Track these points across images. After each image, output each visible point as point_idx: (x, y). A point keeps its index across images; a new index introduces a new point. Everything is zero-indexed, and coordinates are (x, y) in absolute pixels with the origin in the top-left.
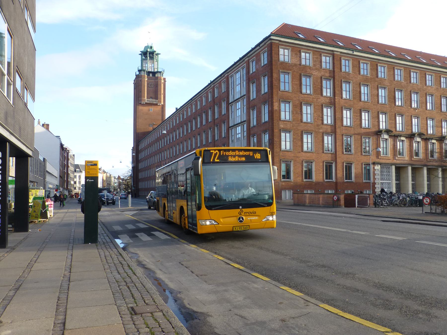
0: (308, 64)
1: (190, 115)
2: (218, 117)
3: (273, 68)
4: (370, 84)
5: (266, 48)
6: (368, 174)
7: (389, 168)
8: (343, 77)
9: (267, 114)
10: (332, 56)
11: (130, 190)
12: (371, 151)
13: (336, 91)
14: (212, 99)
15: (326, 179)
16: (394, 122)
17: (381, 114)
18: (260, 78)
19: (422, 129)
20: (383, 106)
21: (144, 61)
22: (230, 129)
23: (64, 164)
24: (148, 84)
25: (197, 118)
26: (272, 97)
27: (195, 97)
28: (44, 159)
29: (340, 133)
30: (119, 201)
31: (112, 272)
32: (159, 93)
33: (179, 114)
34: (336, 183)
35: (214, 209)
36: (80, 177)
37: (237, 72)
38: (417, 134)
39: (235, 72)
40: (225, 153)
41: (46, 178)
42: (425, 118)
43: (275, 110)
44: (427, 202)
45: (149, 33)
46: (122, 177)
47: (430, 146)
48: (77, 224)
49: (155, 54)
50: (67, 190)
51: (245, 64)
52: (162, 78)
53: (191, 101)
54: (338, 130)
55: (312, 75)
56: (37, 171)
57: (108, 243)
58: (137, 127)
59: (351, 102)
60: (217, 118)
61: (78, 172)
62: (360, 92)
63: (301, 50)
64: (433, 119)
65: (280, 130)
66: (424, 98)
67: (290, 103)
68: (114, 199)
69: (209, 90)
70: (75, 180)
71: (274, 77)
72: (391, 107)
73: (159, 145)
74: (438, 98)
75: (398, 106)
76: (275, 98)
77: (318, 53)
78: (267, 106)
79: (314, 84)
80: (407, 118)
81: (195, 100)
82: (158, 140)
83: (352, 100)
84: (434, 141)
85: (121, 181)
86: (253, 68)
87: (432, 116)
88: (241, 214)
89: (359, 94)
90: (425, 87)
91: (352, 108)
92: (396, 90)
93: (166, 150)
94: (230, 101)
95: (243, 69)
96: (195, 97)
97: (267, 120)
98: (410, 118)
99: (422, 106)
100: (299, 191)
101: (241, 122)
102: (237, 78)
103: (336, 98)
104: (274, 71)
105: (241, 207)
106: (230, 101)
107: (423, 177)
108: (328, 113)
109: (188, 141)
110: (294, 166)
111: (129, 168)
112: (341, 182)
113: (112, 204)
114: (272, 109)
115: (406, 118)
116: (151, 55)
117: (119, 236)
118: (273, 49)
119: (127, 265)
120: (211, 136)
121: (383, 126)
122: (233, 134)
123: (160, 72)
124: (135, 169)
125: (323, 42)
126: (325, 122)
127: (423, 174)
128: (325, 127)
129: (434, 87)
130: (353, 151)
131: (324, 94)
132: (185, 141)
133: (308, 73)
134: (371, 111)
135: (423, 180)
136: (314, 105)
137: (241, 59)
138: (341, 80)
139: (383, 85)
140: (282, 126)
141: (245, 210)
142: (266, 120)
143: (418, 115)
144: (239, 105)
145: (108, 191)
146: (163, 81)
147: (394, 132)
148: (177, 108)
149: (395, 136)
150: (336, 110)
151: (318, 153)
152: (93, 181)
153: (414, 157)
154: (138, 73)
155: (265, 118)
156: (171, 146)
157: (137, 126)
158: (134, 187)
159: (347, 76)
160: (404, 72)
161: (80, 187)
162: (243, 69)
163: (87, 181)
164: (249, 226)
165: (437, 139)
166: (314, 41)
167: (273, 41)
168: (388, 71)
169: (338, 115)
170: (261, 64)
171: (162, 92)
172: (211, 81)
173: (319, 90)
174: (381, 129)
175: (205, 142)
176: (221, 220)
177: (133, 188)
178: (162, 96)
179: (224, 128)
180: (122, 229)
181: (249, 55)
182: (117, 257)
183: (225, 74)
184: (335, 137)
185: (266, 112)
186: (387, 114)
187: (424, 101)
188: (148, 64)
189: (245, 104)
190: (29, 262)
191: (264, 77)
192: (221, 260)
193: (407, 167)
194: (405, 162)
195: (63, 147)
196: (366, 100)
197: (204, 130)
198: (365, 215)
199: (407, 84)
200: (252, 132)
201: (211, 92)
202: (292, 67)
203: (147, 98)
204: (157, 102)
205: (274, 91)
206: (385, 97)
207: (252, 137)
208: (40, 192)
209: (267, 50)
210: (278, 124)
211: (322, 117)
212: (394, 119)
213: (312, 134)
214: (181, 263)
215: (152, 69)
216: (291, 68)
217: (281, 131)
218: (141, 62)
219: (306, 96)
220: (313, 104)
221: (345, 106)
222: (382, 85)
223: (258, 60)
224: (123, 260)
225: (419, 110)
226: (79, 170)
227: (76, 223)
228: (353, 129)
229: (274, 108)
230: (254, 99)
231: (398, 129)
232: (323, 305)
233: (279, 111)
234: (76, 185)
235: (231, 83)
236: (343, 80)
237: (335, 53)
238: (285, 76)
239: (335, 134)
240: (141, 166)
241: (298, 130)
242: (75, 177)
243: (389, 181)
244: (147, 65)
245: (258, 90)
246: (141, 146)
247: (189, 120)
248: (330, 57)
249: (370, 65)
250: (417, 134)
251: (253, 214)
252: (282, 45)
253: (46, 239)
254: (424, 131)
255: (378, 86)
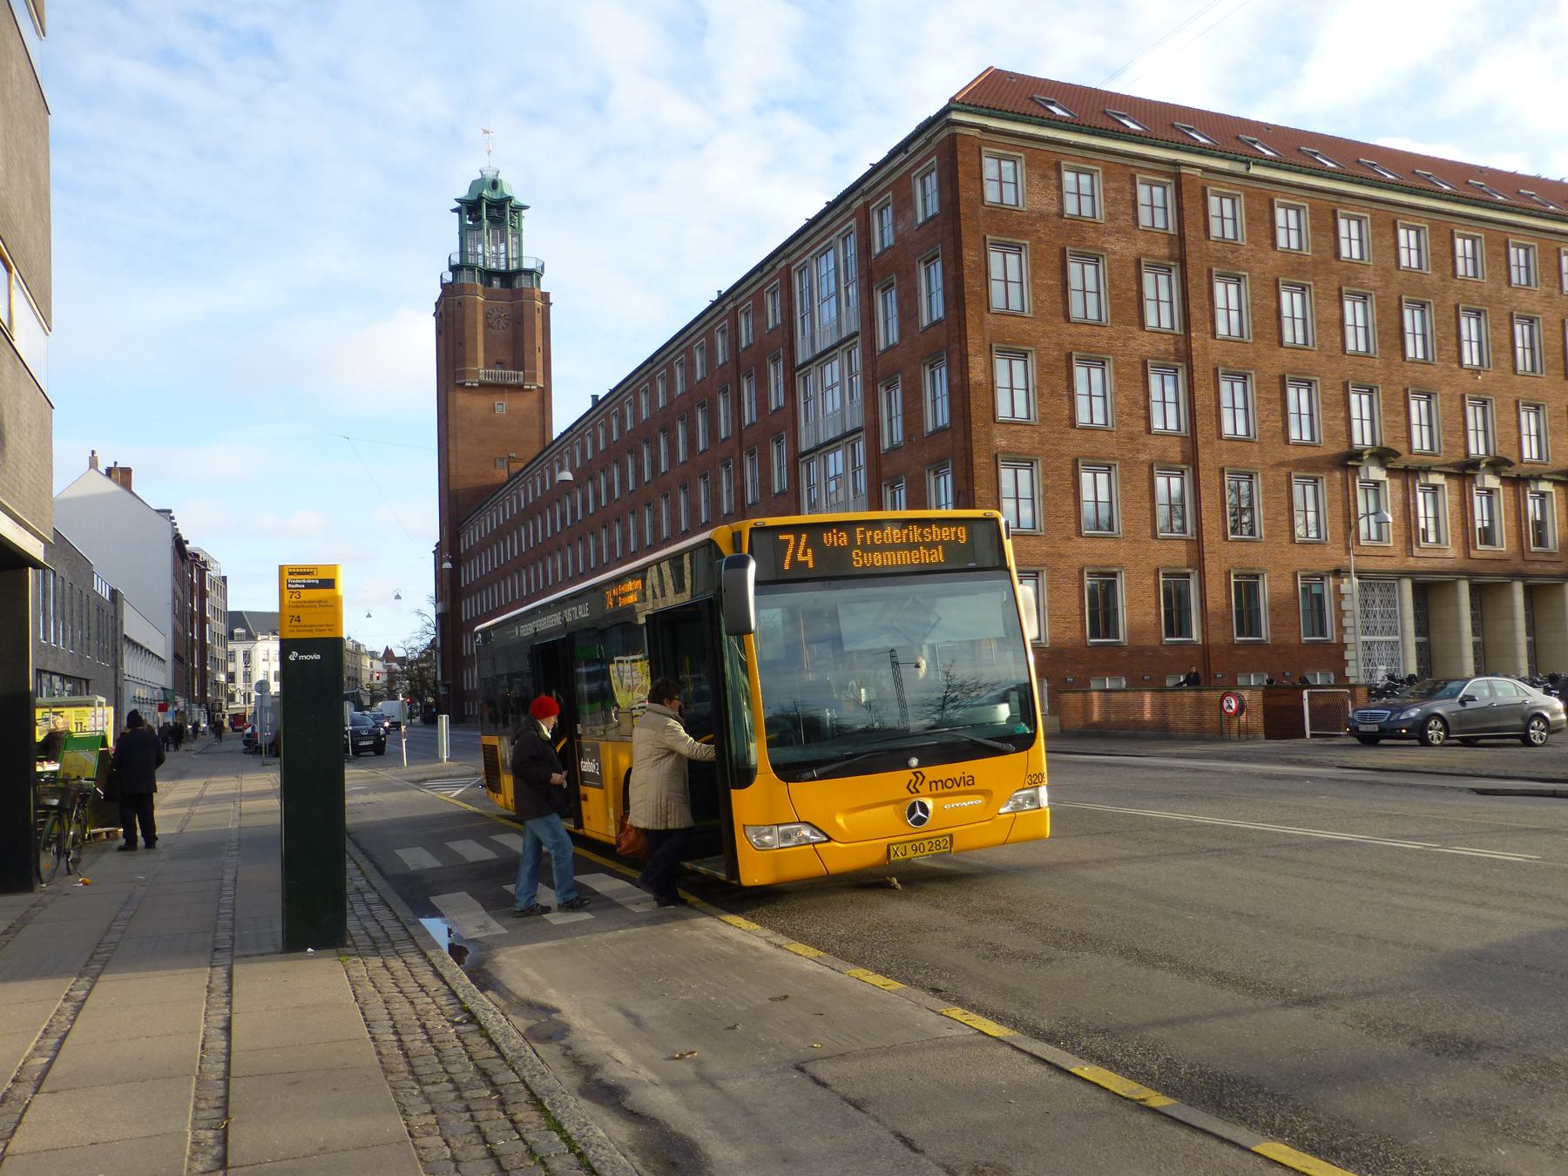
0: (1086, 212)
1: (647, 419)
2: (754, 419)
3: (963, 230)
4: (1311, 283)
5: (934, 158)
6: (1316, 613)
7: (1390, 588)
8: (1213, 259)
9: (945, 398)
10: (1173, 182)
11: (431, 700)
12: (436, 661)
13: (1193, 310)
14: (730, 355)
15: (1168, 635)
16: (1401, 419)
17: (1355, 392)
18: (914, 270)
19: (1501, 443)
20: (1360, 361)
21: (469, 235)
22: (801, 460)
23: (189, 611)
24: (487, 316)
25: (675, 429)
26: (962, 337)
27: (665, 353)
28: (114, 593)
29: (1214, 462)
30: (404, 740)
31: (460, 1155)
32: (527, 346)
33: (607, 416)
34: (1205, 649)
35: (808, 775)
36: (249, 658)
37: (824, 252)
38: (1487, 463)
39: (814, 251)
40: (872, 537)
41: (122, 662)
42: (1511, 402)
43: (976, 383)
44: (1231, 708)
45: (486, 132)
46: (399, 653)
47: (1533, 507)
48: (248, 843)
49: (509, 208)
50: (204, 705)
51: (853, 222)
52: (537, 291)
53: (650, 366)
54: (1204, 455)
55: (1104, 254)
56: (88, 639)
57: (393, 944)
58: (453, 471)
59: (1247, 348)
60: (752, 424)
61: (241, 638)
62: (1279, 311)
63: (1063, 163)
64: (1537, 408)
65: (996, 456)
66: (1506, 330)
67: (1026, 357)
68: (382, 733)
69: (717, 324)
70: (231, 668)
71: (966, 263)
72: (1390, 364)
73: (536, 531)
74: (1554, 328)
75: (1415, 361)
76: (974, 342)
77: (1123, 173)
78: (944, 369)
79: (1113, 285)
80: (1447, 404)
81: (753, 290)
82: (531, 512)
83: (1251, 341)
84: (1545, 486)
85: (395, 666)
86: (884, 234)
87: (1535, 397)
88: (918, 792)
89: (1274, 322)
90: (1506, 291)
91: (1253, 372)
92: (1404, 304)
93: (559, 550)
94: (800, 361)
95: (844, 240)
96: (665, 353)
97: (900, 439)
98: (1457, 403)
99: (1497, 360)
100: (1147, 680)
101: (846, 435)
102: (824, 272)
103: (1193, 335)
104: (965, 240)
105: (914, 762)
106: (800, 361)
107: (1513, 618)
108: (1164, 393)
109: (642, 514)
110: (1050, 591)
111: (425, 618)
112: (1223, 643)
113: (372, 753)
114: (962, 380)
115: (1442, 405)
116: (495, 213)
117: (433, 899)
118: (960, 158)
119: (524, 1096)
120: (729, 491)
121: (1362, 436)
122: (814, 479)
123: (530, 272)
124: (450, 622)
125: (1137, 130)
126: (1157, 425)
127: (1512, 608)
128: (1158, 442)
129: (1539, 290)
130: (1261, 530)
131: (1151, 321)
132: (633, 513)
133: (1090, 247)
134: (1321, 383)
135: (1513, 630)
136: (1115, 362)
137: (831, 206)
138: (1210, 271)
139: (1359, 287)
140: (1002, 443)
141: (933, 772)
142: (940, 424)
143: (1487, 394)
144: (833, 371)
145: (353, 702)
146: (539, 304)
147: (1405, 455)
148: (595, 397)
149: (1409, 473)
150: (1195, 380)
151: (1136, 541)
152: (318, 657)
153: (1479, 547)
154: (449, 277)
155: (938, 413)
156: (577, 533)
157: (452, 468)
158: (447, 686)
159: (1230, 255)
160: (1430, 239)
161: (249, 694)
162: (844, 240)
163: (292, 658)
164: (951, 836)
165: (1555, 477)
166: (1107, 129)
167: (959, 130)
168: (1374, 236)
169: (1203, 398)
170: (916, 219)
171: (539, 342)
172: (719, 292)
173: (1130, 306)
174: (1356, 447)
175: (687, 522)
176: (840, 820)
177: (442, 691)
178: (539, 356)
179: (778, 458)
180: (438, 864)
181: (865, 186)
182: (458, 1037)
183: (776, 260)
184: (1194, 478)
185: (938, 394)
186: (1375, 390)
187: (1507, 342)
188: (486, 245)
189: (857, 364)
190: (8, 1084)
191: (926, 263)
192: (999, 1040)
193: (1454, 583)
194: (1447, 564)
195: (184, 549)
196: (1300, 340)
197: (702, 468)
198: (1378, 766)
199: (1442, 280)
200: (886, 470)
201: (682, 364)
202: (1031, 225)
203: (487, 366)
204: (521, 380)
205: (969, 312)
206: (1366, 328)
207: (888, 488)
208: (95, 717)
209: (894, 199)
210: (989, 435)
211: (1147, 408)
212: (1402, 409)
213: (1113, 469)
214: (809, 1067)
215: (498, 263)
216: (1028, 228)
217: (999, 460)
218: (461, 239)
219: (1085, 329)
220: (1111, 357)
221: (1225, 364)
222: (1354, 286)
223: (904, 203)
224: (493, 1053)
225: (1491, 374)
226: (244, 631)
227: (239, 840)
228: (1256, 447)
229: (970, 375)
230: (890, 348)
231: (1416, 445)
232: (1088, 1071)
233: (990, 387)
234: (234, 687)
235: (801, 292)
236: (1214, 269)
237: (1182, 171)
238: (1008, 256)
239: (1194, 468)
240: (468, 609)
241: (1062, 456)
242: (231, 656)
243: (1393, 634)
244: (480, 249)
245: (908, 313)
246: (469, 539)
247: (645, 435)
248: (1165, 188)
249: (1310, 213)
250: (1487, 463)
251: (962, 788)
252: (992, 144)
253: (108, 931)
254: (1507, 452)
255: (1340, 290)
